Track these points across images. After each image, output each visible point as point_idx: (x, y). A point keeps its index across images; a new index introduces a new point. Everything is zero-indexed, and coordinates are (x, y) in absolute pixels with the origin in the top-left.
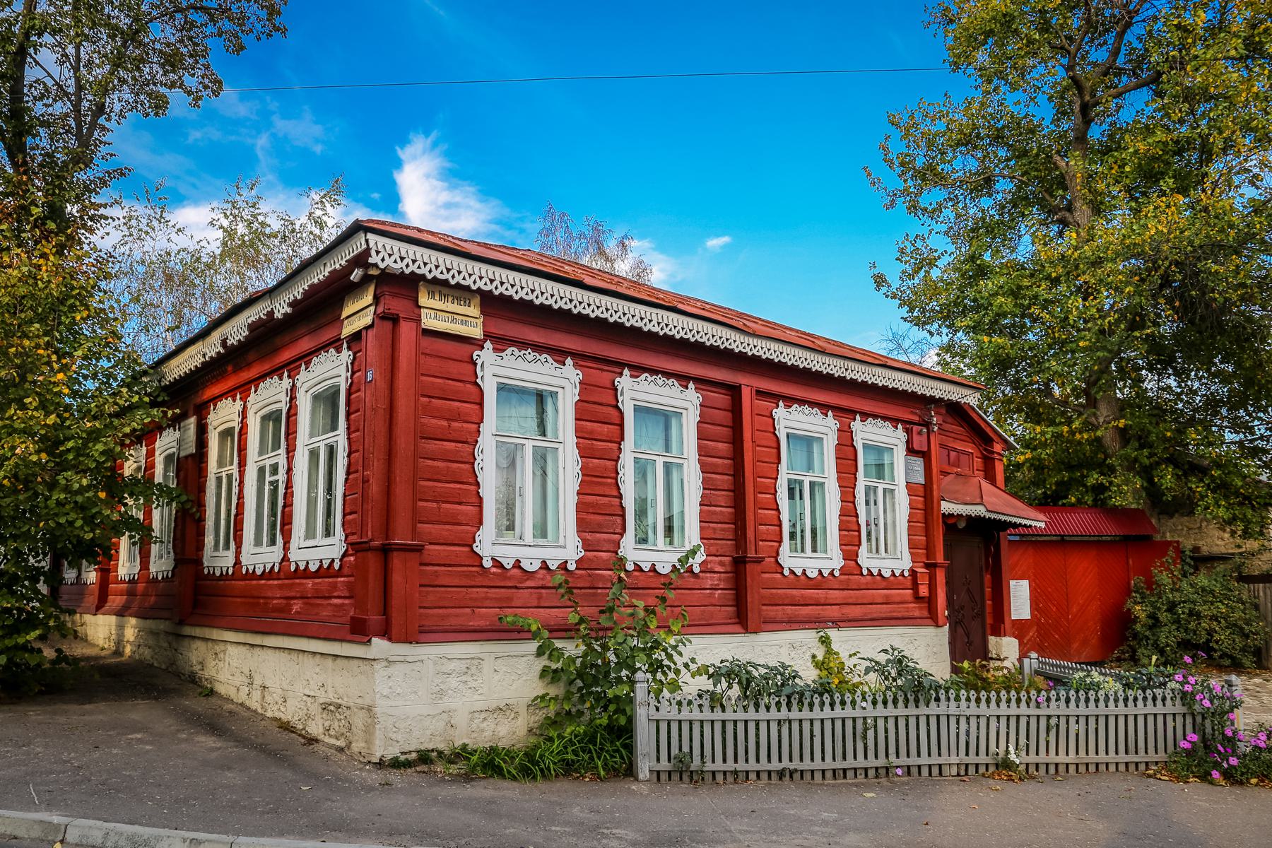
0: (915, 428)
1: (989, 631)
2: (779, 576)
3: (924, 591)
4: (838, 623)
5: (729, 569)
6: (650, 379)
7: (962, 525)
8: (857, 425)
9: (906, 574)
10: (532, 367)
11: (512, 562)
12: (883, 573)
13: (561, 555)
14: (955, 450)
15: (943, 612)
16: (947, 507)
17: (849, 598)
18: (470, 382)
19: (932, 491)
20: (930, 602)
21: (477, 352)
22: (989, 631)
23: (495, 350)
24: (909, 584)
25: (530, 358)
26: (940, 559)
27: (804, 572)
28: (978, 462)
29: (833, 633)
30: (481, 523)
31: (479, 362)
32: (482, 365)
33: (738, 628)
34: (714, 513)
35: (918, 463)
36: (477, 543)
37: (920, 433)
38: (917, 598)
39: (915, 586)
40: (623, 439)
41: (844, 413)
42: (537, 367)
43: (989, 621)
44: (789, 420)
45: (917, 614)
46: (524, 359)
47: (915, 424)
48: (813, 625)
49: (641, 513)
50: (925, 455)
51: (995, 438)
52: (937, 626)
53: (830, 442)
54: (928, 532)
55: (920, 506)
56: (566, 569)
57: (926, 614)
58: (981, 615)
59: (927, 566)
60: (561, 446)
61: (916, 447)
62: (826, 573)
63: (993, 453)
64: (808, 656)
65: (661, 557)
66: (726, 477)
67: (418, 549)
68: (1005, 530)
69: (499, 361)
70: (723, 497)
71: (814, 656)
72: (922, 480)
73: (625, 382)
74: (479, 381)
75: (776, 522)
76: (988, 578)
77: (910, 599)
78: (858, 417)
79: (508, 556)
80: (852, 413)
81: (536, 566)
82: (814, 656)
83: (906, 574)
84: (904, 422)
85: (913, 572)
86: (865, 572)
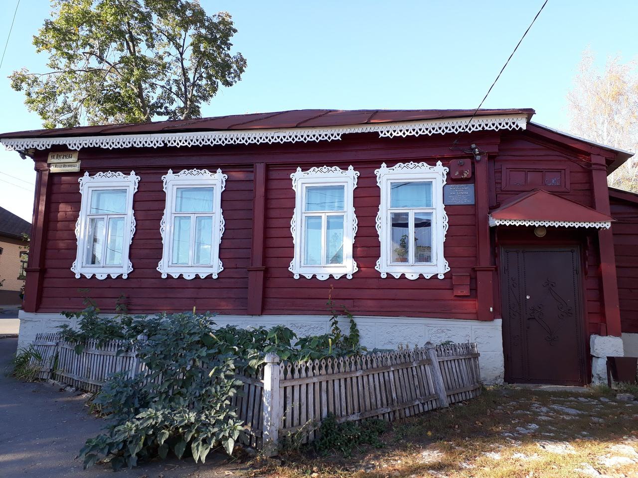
60: (303, 211)
79: (397, 271)
81: (105, 277)
84: (442, 159)
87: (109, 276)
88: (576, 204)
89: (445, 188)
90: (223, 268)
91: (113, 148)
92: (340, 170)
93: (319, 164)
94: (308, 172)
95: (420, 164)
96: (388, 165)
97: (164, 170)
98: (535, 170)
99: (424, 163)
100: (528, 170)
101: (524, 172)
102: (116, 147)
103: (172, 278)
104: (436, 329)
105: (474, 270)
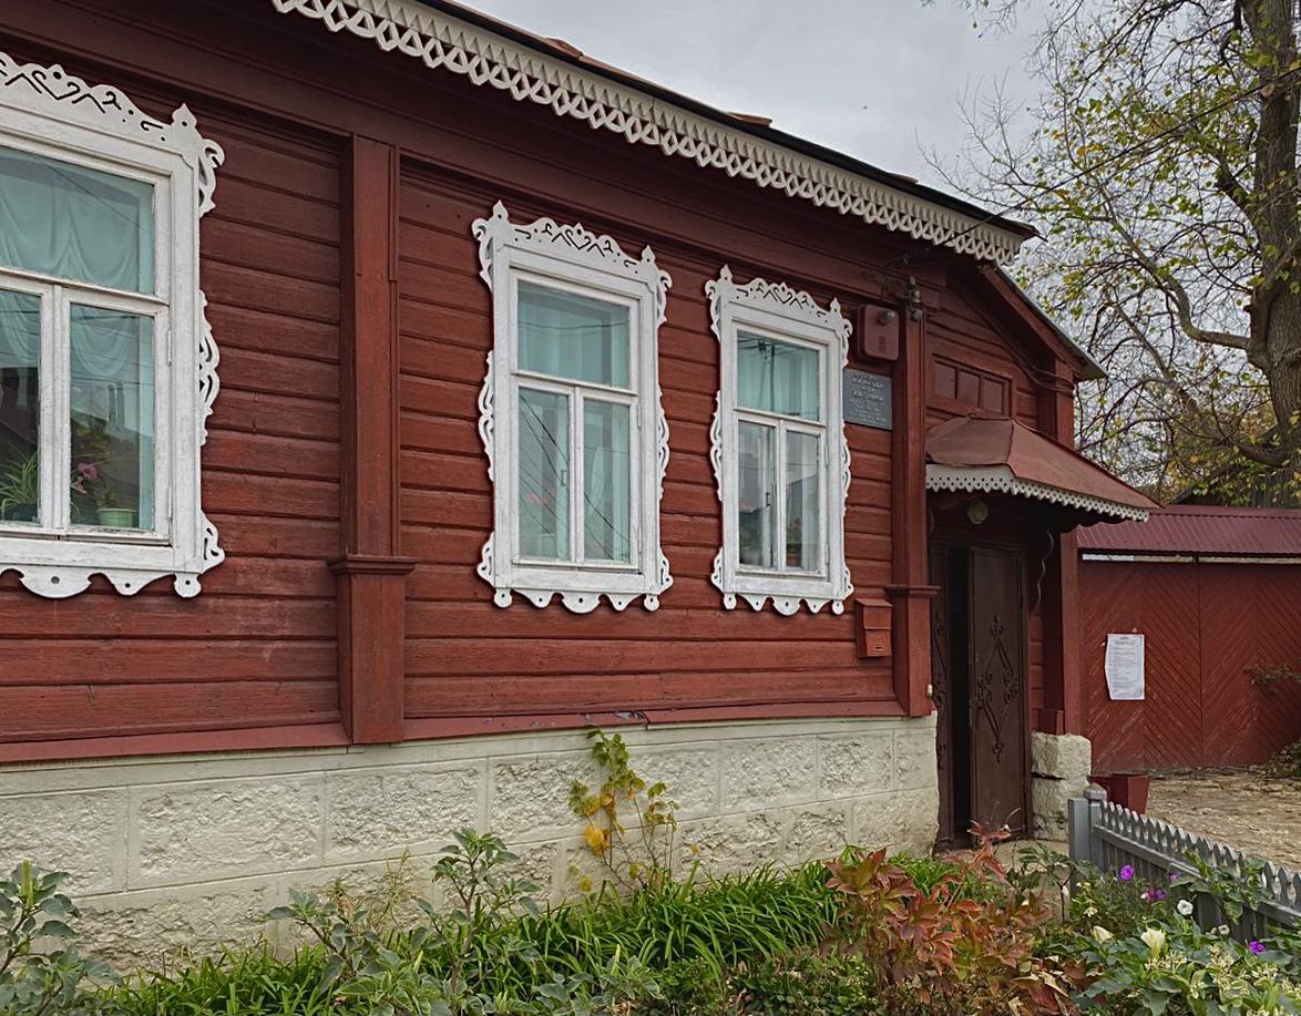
0: (871, 310)
1: (1032, 722)
2: (483, 607)
3: (879, 645)
4: (642, 717)
5: (310, 588)
6: (766, 288)
7: (978, 516)
8: (722, 289)
9: (838, 609)
10: (66, 109)
11: (762, 601)
12: (779, 605)
13: (161, 561)
14: (971, 370)
15: (921, 679)
16: (937, 478)
17: (684, 659)
18: (467, 274)
19: (905, 443)
20: (896, 665)
21: (710, 283)
22: (1032, 722)
23: (512, 218)
24: (845, 629)
25: (580, 240)
26: (918, 578)
27: (557, 599)
28: (1021, 400)
29: (635, 741)
30: (490, 529)
31: (484, 240)
32: (489, 247)
33: (330, 735)
34: (272, 451)
35: (878, 390)
36: (717, 572)
37: (880, 320)
38: (863, 658)
39: (859, 636)
40: (491, 347)
41: (689, 261)
42: (793, 310)
43: (1033, 702)
44: (515, 252)
45: (861, 692)
46: (570, 242)
47: (873, 302)
48: (578, 720)
49: (749, 520)
50: (893, 370)
51: (1059, 352)
52: (908, 715)
53: (648, 319)
54: (895, 529)
55: (880, 474)
56: (831, 613)
57: (887, 692)
58: (1019, 692)
59: (890, 594)
60: (634, 403)
61: (871, 349)
62: (620, 604)
63: (1054, 380)
64: (559, 788)
65: (788, 591)
66: (883, 459)
67: (401, 570)
68: (1070, 528)
69: (523, 242)
70: (878, 492)
71: (577, 790)
72: (885, 421)
73: (495, 229)
74: (484, 274)
75: (480, 485)
76: (1033, 623)
77: (848, 660)
78: (725, 272)
79: (539, 585)
80: (712, 263)
81: (591, 604)
82: (577, 790)
83: (838, 609)
84: (843, 296)
85: (852, 604)
86: (730, 603)
87: (605, 600)
88: (73, 291)
89: (482, 292)
90: (221, 553)
91: (442, 66)
92: (816, 306)
93: (564, 215)
94: (529, 228)
95: (101, 91)
96: (205, 121)
97: (484, 194)
98: (969, 369)
99: (121, 97)
100: (986, 375)
101: (953, 370)
102: (613, 127)
103: (111, 590)
104: (835, 744)
105: (339, 572)
